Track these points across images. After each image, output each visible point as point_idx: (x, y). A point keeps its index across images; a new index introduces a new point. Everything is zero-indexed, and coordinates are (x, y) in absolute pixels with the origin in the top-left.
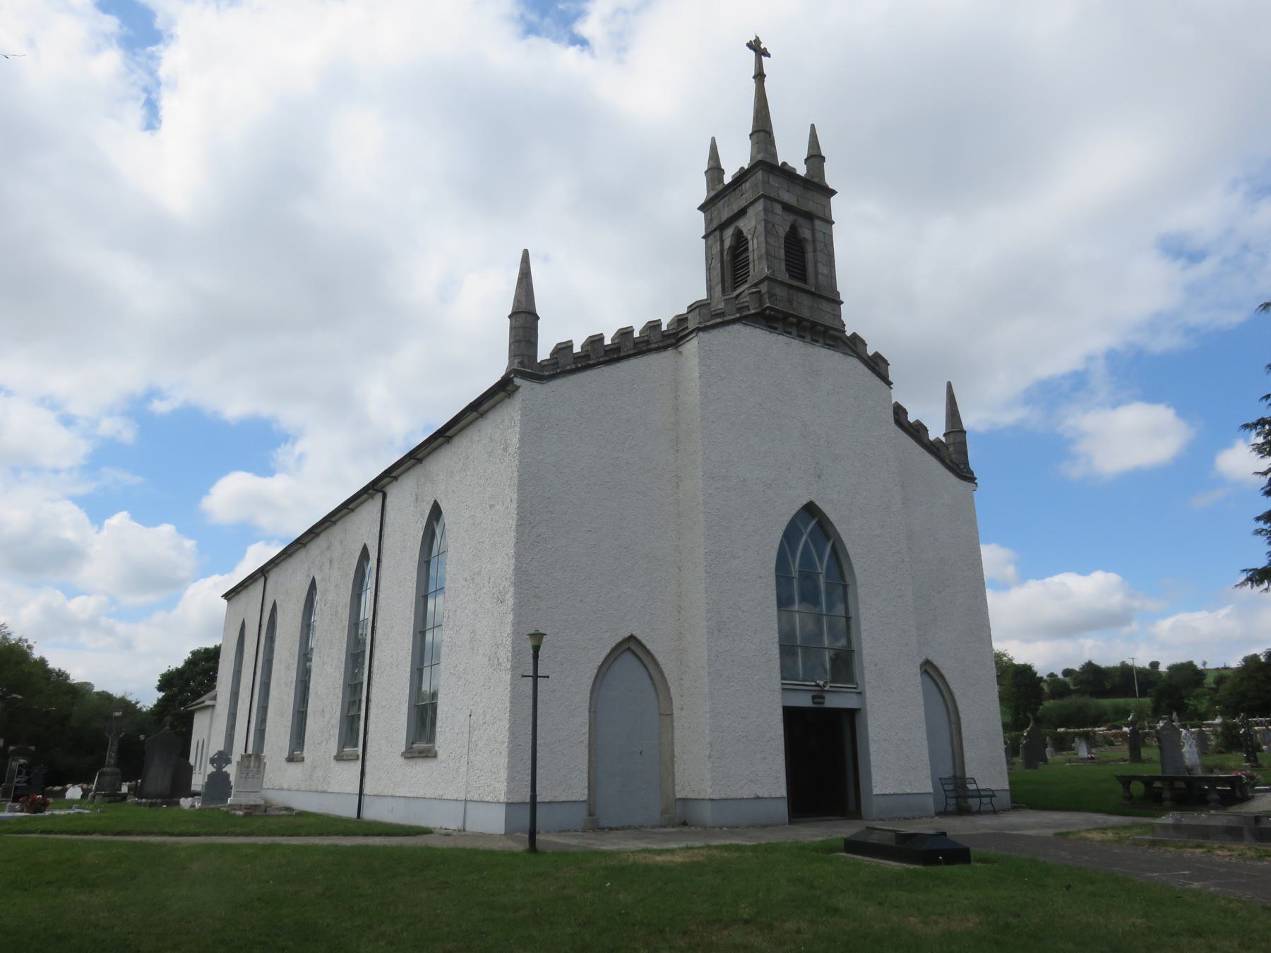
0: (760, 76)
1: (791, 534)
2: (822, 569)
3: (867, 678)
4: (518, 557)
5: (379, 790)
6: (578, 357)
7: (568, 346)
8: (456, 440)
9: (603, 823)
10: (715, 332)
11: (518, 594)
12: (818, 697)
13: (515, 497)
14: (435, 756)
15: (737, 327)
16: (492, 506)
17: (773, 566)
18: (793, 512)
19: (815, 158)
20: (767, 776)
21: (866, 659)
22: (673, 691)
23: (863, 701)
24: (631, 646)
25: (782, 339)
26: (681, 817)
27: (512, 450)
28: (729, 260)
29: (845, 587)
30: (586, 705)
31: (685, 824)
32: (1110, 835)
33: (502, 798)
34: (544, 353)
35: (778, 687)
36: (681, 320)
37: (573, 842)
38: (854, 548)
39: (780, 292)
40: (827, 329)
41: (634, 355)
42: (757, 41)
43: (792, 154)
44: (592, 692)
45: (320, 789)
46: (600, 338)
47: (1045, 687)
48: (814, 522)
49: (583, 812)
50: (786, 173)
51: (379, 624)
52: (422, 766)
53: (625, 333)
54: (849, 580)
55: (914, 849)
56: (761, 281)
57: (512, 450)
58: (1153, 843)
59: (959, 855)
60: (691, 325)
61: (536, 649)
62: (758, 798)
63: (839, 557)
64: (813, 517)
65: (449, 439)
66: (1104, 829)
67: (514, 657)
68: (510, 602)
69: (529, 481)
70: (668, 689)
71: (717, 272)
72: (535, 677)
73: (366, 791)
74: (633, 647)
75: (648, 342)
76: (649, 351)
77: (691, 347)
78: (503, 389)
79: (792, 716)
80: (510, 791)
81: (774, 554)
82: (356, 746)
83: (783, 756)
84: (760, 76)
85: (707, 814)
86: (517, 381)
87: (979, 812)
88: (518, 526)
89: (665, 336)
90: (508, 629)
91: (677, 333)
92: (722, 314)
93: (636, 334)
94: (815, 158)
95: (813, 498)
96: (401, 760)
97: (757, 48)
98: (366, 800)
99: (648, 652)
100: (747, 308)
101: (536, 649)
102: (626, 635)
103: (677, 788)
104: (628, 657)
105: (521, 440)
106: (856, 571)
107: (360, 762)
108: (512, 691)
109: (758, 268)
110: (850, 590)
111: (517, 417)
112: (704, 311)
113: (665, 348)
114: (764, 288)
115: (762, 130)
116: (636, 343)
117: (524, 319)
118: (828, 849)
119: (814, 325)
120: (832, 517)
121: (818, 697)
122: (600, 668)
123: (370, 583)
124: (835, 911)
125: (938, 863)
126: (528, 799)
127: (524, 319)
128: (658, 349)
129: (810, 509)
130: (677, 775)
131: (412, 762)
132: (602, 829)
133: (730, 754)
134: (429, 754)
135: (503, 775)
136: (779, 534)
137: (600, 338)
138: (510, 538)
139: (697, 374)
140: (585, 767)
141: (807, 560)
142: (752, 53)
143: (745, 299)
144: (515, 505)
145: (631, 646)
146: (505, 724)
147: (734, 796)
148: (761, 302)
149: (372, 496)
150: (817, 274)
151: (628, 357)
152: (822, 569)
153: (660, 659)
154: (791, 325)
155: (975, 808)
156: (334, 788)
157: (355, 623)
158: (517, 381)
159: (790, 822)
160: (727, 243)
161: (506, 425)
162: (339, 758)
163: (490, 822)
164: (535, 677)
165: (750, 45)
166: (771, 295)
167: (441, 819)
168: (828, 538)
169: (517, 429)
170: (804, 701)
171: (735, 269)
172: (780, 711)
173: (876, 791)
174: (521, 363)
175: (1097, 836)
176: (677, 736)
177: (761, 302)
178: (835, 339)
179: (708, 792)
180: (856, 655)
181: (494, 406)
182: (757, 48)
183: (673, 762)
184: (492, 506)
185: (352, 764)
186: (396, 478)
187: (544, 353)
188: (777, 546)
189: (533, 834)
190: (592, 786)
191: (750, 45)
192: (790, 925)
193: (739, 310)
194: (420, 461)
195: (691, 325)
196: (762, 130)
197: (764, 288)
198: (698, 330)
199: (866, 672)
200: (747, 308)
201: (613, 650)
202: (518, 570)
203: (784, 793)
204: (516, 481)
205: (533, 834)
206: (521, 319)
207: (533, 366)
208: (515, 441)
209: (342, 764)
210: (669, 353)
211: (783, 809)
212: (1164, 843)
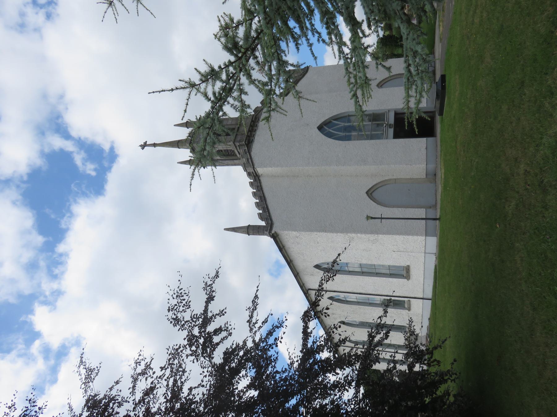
0: (155, 145)
1: (329, 135)
2: (342, 124)
3: (383, 108)
4: (337, 232)
5: (421, 290)
6: (264, 211)
7: (260, 215)
8: (291, 258)
9: (434, 203)
10: (254, 162)
11: (351, 232)
12: (390, 126)
13: (315, 233)
14: (409, 266)
15: (252, 154)
16: (318, 243)
17: (341, 142)
18: (321, 134)
19: (187, 125)
20: (419, 144)
21: (376, 108)
22: (387, 179)
23: (392, 109)
24: (370, 193)
25: (256, 138)
26: (432, 176)
27: (298, 235)
28: (228, 157)
29: (349, 116)
30: (391, 209)
31: (435, 175)
32: (441, 24)
33: (424, 238)
34: (263, 223)
35: (386, 141)
36: (249, 174)
37: (439, 210)
38: (335, 112)
39: (239, 138)
40: (252, 121)
41: (262, 191)
42: (141, 146)
43: (183, 134)
44: (386, 207)
45: (421, 318)
46: (256, 203)
47: (387, 33)
48: (325, 127)
49: (429, 210)
50: (191, 135)
51: (359, 292)
52: (413, 272)
53: (254, 194)
54: (347, 114)
55: (441, 95)
56: (235, 145)
57: (298, 235)
58: (443, 11)
59: (443, 77)
60: (251, 170)
61: (372, 218)
62: (426, 148)
63: (337, 118)
64: (323, 127)
65: (291, 261)
66: (439, 25)
67: (373, 234)
68: (354, 235)
69: (310, 228)
70: (386, 180)
71: (229, 162)
72: (381, 218)
73: (422, 297)
74: (370, 192)
75: (258, 187)
76: (261, 186)
77: (260, 171)
78: (275, 237)
79: (397, 136)
80: (422, 235)
81: (337, 141)
82: (404, 301)
83: (411, 139)
84: (155, 145)
85: (431, 166)
86: (273, 232)
87: (435, 67)
88: (326, 232)
89: (255, 180)
90: (363, 236)
91: (254, 176)
92: (248, 159)
93: (255, 191)
94: (187, 125)
95: (316, 127)
96: (410, 281)
97: (144, 146)
98: (425, 297)
99: (374, 186)
100: (245, 150)
101: (372, 218)
102: (366, 195)
103: (422, 177)
104: (374, 194)
105: (295, 231)
106: (343, 111)
107: (410, 299)
108: (386, 234)
109: (230, 146)
110: (350, 114)
111: (286, 232)
112: (246, 165)
113: (260, 180)
114: (237, 144)
115: (177, 144)
116: (258, 190)
117: (250, 230)
118: (442, 121)
119: (251, 126)
120: (323, 120)
121: (390, 126)
122: (378, 204)
123: (342, 296)
124: (454, 117)
125: (445, 85)
126: (424, 221)
127: (250, 230)
128: (260, 183)
129: (320, 128)
130: (417, 177)
131: (411, 276)
132: (436, 203)
133: (411, 158)
134: (408, 269)
135: (415, 237)
136: (329, 139)
137: (256, 203)
138: (330, 235)
139: (270, 169)
140: (414, 209)
141: (339, 130)
142: (146, 148)
143: (241, 151)
144: (318, 233)
145: (370, 193)
146: (397, 237)
147: (425, 157)
148: (243, 145)
149: (309, 295)
150: (231, 125)
151: (263, 193)
152: (342, 124)
153: (375, 183)
154: (251, 134)
155: (433, 68)
156: (420, 311)
157: (358, 303)
158: (273, 232)
159: (436, 137)
160: (218, 158)
161: (288, 237)
162: (409, 309)
163: (433, 242)
164: (381, 218)
165: (143, 149)
166: (240, 141)
167: (432, 261)
168: (330, 122)
169: (290, 232)
170: (391, 131)
171: (228, 155)
172: (395, 140)
173: (425, 105)
174: (266, 231)
175: (441, 28)
176: (403, 177)
177: (243, 145)
178: (256, 118)
179: (424, 166)
180: (375, 112)
181: (281, 242)
182: (144, 146)
183: (413, 179)
184: (318, 243)
185: (411, 303)
186: (303, 284)
187: (263, 223)
188: (333, 140)
189: (435, 219)
190: (421, 207)
191: (143, 149)
192: (457, 129)
193: (246, 153)
194: (298, 273)
195: (251, 170)
196: (177, 144)
197: (237, 144)
198: (254, 168)
199: (381, 108)
200: (245, 150)
201: (371, 199)
202: (342, 232)
203: (425, 139)
204: (309, 233)
205: (435, 219)
206: (251, 231)
207: (267, 226)
208: (295, 233)
209: (412, 308)
210: (261, 178)
211: (431, 139)
212: (443, 7)
